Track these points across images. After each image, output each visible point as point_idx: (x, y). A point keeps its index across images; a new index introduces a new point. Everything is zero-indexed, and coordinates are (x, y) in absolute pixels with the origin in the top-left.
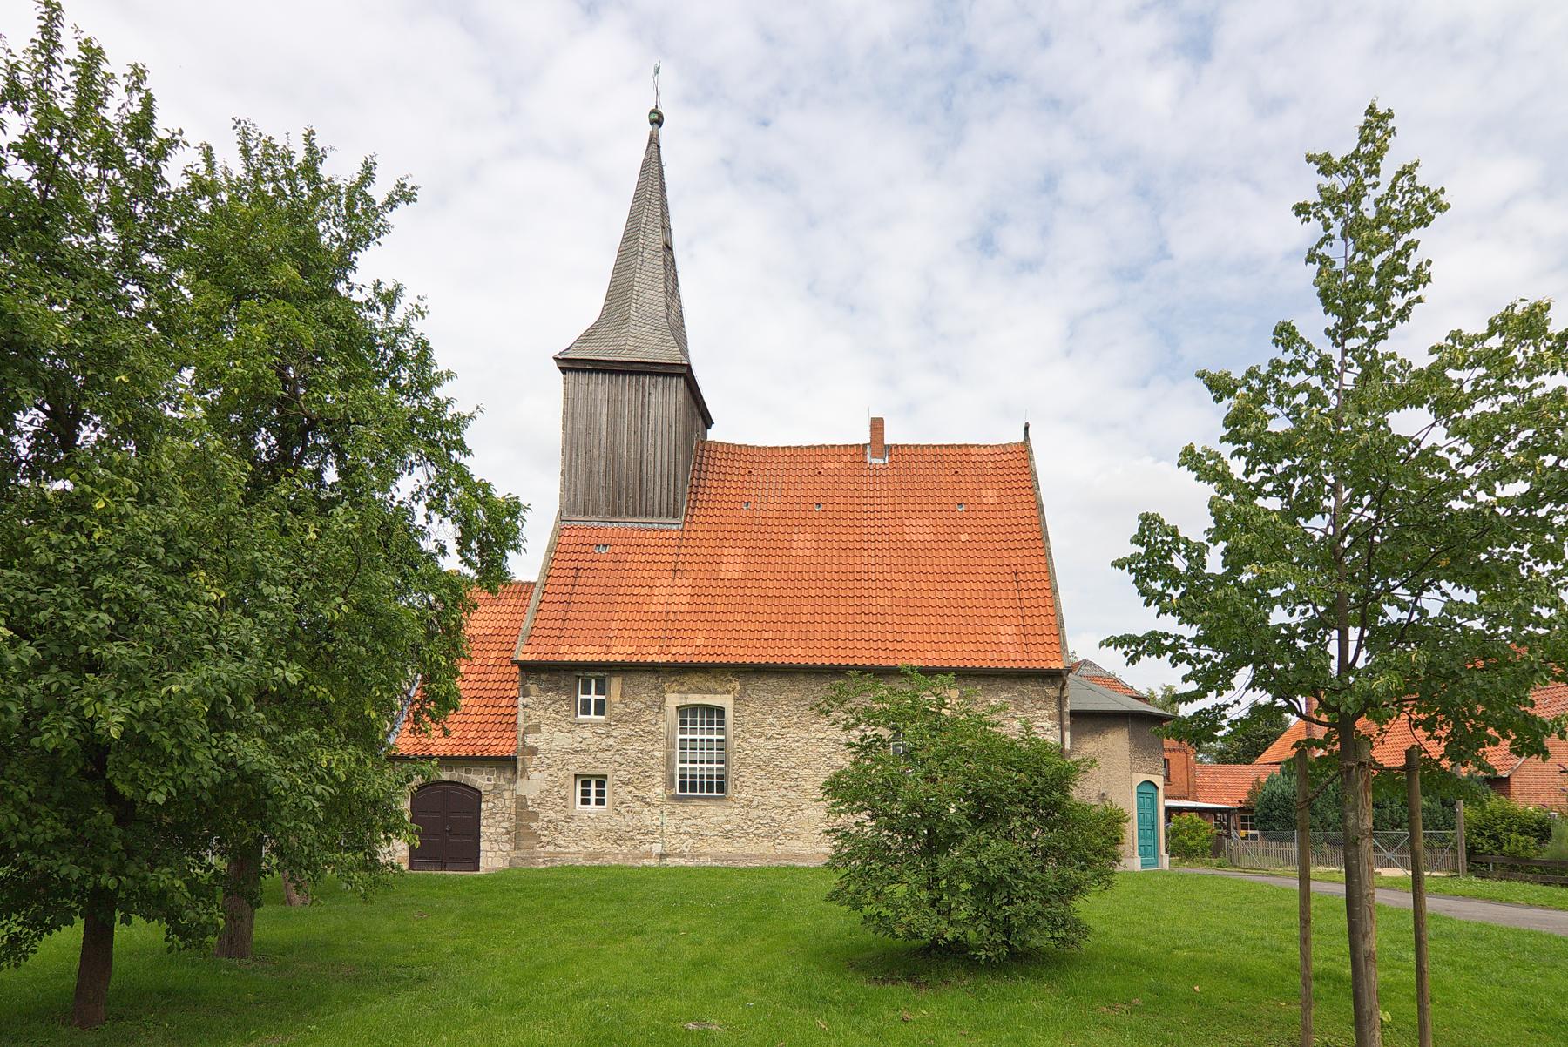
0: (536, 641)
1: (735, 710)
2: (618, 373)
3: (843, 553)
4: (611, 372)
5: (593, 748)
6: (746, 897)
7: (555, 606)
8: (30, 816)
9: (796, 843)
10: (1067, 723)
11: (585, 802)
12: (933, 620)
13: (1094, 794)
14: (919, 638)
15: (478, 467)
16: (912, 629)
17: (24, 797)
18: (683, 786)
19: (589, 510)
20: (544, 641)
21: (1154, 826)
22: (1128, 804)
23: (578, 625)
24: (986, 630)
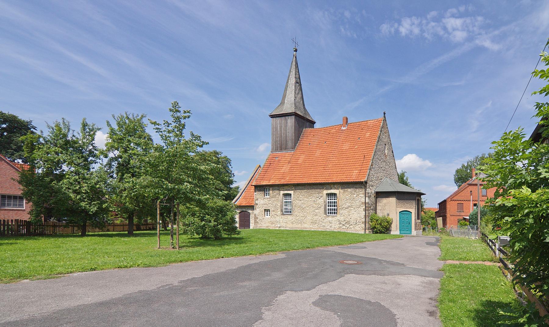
2: (281, 117)
13: (386, 214)
19: (277, 150)
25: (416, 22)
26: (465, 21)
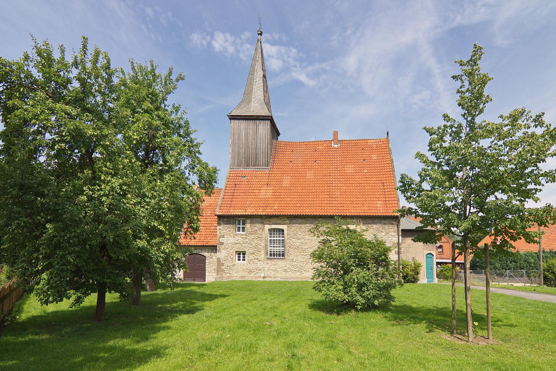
0: (222, 208)
1: (288, 230)
2: (248, 119)
3: (324, 177)
4: (246, 119)
5: (241, 242)
6: (290, 290)
7: (228, 197)
8: (87, 263)
9: (308, 273)
10: (400, 234)
11: (239, 260)
12: (354, 199)
13: (411, 258)
14: (349, 205)
15: (203, 158)
16: (347, 202)
17: (86, 258)
18: (271, 255)
19: (239, 165)
20: (225, 208)
21: (432, 269)
22: (422, 260)
23: (236, 203)
24: (372, 202)
25: (231, 39)
26: (280, 50)
